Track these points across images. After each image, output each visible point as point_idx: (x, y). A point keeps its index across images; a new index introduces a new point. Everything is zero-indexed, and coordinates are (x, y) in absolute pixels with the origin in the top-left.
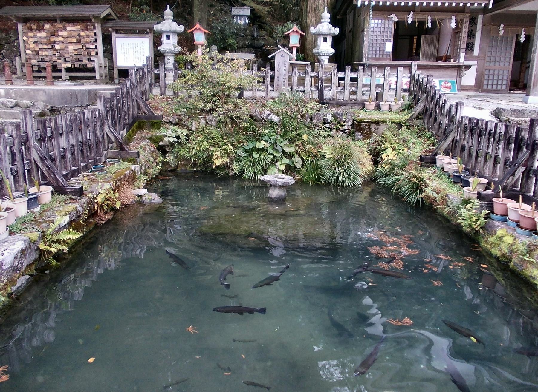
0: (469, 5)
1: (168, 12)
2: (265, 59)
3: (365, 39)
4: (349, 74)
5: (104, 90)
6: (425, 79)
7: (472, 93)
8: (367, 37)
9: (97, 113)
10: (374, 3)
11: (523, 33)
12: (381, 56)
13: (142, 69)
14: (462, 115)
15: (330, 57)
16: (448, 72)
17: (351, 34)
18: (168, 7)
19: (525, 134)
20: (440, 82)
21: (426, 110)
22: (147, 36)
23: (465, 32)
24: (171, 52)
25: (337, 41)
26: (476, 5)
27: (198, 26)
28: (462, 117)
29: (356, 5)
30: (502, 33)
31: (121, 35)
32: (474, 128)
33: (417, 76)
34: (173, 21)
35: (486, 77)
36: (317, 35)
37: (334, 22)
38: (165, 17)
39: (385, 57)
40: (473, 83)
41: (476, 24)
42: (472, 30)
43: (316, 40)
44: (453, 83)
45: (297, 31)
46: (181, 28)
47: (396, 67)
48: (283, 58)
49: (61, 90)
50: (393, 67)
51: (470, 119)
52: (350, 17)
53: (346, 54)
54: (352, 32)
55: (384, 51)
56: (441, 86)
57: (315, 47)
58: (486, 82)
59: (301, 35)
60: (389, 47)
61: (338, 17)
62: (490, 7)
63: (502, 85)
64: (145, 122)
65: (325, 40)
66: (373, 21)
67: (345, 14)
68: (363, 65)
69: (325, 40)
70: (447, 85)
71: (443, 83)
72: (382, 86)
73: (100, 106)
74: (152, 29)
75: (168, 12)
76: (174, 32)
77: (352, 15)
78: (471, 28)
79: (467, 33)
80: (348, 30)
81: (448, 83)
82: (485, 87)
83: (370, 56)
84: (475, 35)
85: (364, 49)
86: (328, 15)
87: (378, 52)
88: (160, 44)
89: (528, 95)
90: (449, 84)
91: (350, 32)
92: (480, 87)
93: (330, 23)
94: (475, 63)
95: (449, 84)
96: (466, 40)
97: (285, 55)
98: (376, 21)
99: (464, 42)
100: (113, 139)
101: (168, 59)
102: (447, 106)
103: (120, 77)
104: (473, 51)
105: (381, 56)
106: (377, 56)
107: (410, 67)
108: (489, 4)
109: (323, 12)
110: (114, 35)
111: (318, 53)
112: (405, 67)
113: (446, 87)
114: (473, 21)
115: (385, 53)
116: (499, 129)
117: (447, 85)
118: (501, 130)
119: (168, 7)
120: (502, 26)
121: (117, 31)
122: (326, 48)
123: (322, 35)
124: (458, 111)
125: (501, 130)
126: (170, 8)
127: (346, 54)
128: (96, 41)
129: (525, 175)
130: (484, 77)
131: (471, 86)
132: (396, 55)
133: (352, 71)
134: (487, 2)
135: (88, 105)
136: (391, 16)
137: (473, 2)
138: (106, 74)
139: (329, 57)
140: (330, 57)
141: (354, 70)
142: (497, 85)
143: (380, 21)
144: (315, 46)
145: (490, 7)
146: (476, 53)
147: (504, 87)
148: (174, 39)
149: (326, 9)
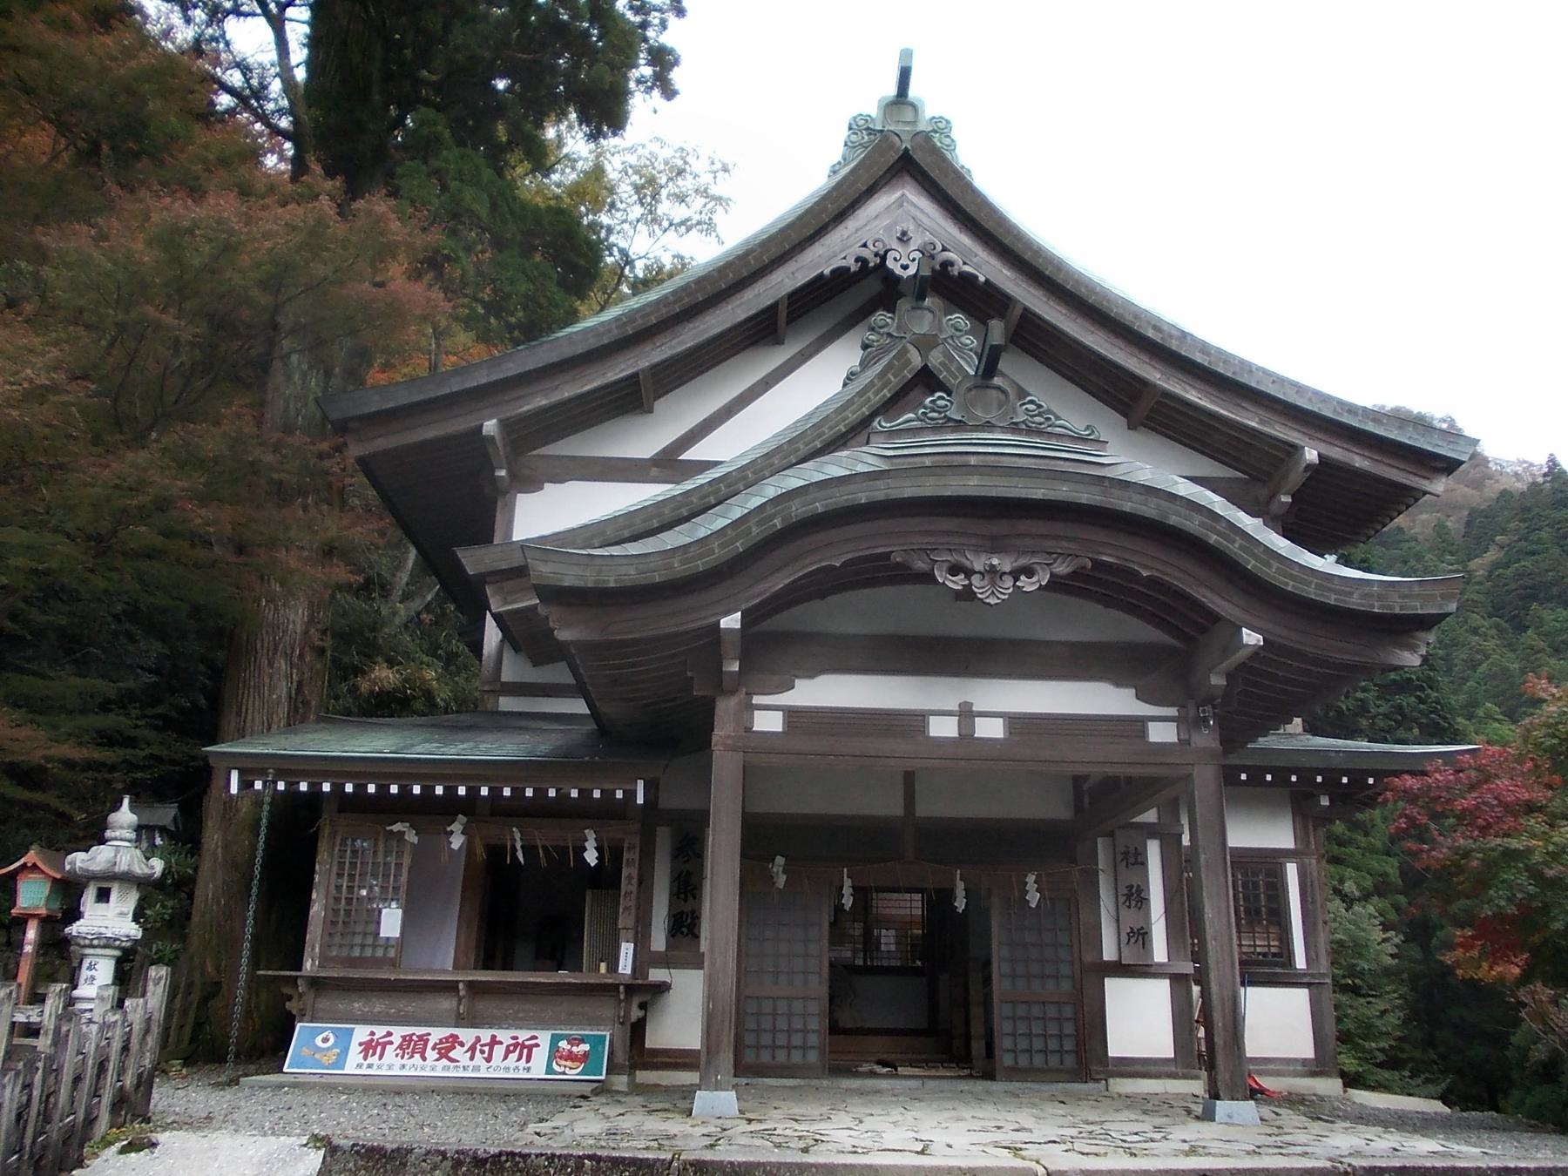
3: (314, 896)
8: (322, 890)
11: (847, 883)
16: (590, 1006)
20: (555, 1040)
24: (108, 943)
30: (781, 880)
42: (689, 874)
44: (597, 1042)
62: (640, 801)
70: (575, 1049)
71: (563, 1044)
76: (127, 878)
81: (582, 1041)
85: (311, 928)
99: (626, 908)
101: (90, 968)
104: (697, 937)
113: (571, 1057)
117: (575, 1049)
119: (126, 801)
120: (780, 860)
126: (131, 802)
136: (397, 827)
137: (587, 786)
147: (813, 1057)
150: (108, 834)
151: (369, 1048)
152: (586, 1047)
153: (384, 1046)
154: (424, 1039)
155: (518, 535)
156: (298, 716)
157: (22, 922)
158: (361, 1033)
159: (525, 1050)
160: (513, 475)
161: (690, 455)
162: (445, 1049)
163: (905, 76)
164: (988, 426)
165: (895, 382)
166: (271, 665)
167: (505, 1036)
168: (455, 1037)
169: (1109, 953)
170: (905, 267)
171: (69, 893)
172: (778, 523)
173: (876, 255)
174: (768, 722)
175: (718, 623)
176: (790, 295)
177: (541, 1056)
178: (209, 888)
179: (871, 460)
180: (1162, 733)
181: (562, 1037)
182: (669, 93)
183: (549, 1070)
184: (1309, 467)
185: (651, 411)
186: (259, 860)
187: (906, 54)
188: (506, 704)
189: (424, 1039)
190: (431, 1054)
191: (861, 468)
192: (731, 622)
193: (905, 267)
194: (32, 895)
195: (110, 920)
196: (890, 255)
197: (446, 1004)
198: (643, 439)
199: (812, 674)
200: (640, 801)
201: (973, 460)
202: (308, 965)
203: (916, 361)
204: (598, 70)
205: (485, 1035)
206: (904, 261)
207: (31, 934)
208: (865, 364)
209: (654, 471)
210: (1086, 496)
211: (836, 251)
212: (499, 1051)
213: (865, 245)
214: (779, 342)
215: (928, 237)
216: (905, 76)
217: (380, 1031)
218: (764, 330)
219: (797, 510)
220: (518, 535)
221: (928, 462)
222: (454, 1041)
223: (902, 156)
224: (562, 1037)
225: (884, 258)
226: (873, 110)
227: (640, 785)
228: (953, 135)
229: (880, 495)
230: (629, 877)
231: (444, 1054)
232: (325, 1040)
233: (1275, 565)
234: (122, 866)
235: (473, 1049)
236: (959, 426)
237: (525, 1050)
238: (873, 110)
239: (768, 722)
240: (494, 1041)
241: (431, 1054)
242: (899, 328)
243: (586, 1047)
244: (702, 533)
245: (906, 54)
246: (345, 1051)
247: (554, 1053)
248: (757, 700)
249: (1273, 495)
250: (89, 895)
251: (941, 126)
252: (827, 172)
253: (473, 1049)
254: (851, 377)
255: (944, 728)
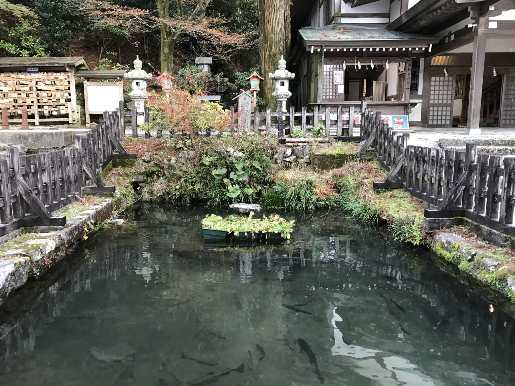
0: (410, 49)
1: (138, 63)
2: (229, 101)
4: (305, 114)
5: (81, 132)
6: (375, 116)
7: (420, 128)
9: (76, 152)
10: (325, 50)
12: (334, 97)
13: (116, 113)
14: (408, 145)
15: (288, 99)
17: (305, 80)
18: (137, 56)
19: (463, 157)
20: (393, 118)
21: (380, 144)
22: (118, 83)
23: (409, 74)
25: (293, 85)
26: (417, 49)
27: (165, 74)
28: (408, 147)
29: (310, 52)
31: (92, 83)
32: (419, 155)
33: (366, 113)
34: (142, 69)
35: (431, 113)
36: (276, 79)
37: (289, 68)
38: (134, 67)
39: (337, 97)
40: (419, 120)
41: (419, 67)
42: (415, 72)
43: (273, 85)
45: (257, 77)
46: (150, 76)
47: (348, 106)
48: (246, 101)
49: (13, 133)
50: (345, 106)
51: (415, 147)
52: (305, 64)
53: (302, 96)
54: (306, 77)
55: (336, 92)
56: (394, 122)
57: (274, 90)
58: (431, 118)
59: (261, 80)
60: (341, 89)
61: (293, 64)
62: (430, 51)
63: (446, 120)
64: (121, 159)
65: (283, 84)
66: (325, 66)
67: (300, 61)
68: (319, 105)
69: (283, 84)
70: (399, 121)
71: (396, 119)
72: (348, 122)
73: (78, 145)
74: (121, 77)
75: (138, 63)
77: (306, 62)
78: (414, 70)
79: (410, 75)
80: (303, 76)
81: (400, 118)
82: (430, 122)
83: (324, 97)
84: (418, 76)
86: (285, 62)
87: (331, 94)
88: (130, 90)
89: (469, 128)
90: (401, 121)
91: (305, 77)
92: (426, 123)
93: (286, 69)
94: (420, 101)
95: (401, 121)
96: (410, 81)
97: (247, 97)
98: (328, 66)
100: (90, 176)
102: (395, 138)
103: (91, 122)
104: (417, 90)
105: (334, 97)
106: (331, 97)
107: (361, 106)
108: (429, 48)
109: (280, 59)
110: (86, 83)
111: (277, 95)
112: (356, 106)
113: (398, 123)
114: (415, 65)
115: (337, 94)
116: (440, 154)
117: (399, 121)
118: (442, 155)
119: (137, 56)
121: (88, 79)
122: (283, 91)
123: (280, 79)
124: (405, 141)
125: (442, 155)
127: (302, 96)
128: (69, 88)
129: (465, 193)
130: (429, 113)
131: (418, 122)
132: (347, 95)
133: (308, 112)
134: (427, 47)
135: (64, 147)
137: (414, 47)
138: (78, 119)
139: (286, 99)
140: (288, 99)
141: (310, 109)
142: (441, 120)
143: (332, 66)
144: (273, 89)
145: (430, 51)
146: (420, 92)
147: (448, 122)
148: (144, 85)
149: (282, 56)
150: (279, 67)
188: (344, 21)
224: (395, 117)
227: (431, 46)
234: (142, 77)
239: (493, 25)
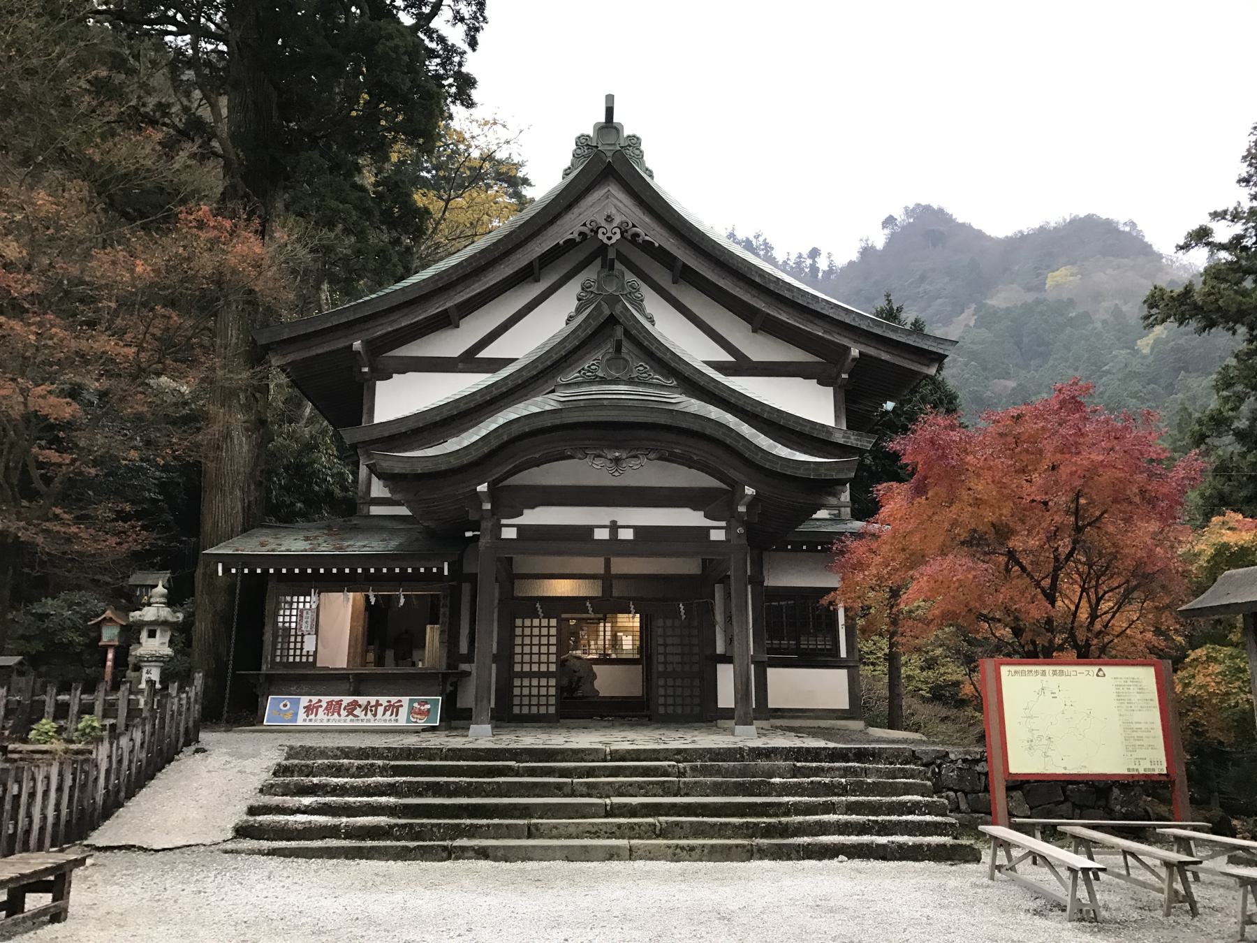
20: (411, 702)
62: (446, 573)
71: (416, 705)
76: (165, 624)
81: (426, 702)
113: (421, 713)
151: (308, 709)
152: (428, 706)
153: (317, 708)
154: (339, 703)
155: (378, 419)
156: (249, 525)
157: (105, 649)
158: (304, 700)
159: (395, 709)
160: (372, 370)
161: (485, 354)
162: (351, 708)
163: (610, 112)
164: (616, 381)
165: (594, 324)
166: (231, 493)
167: (383, 700)
168: (356, 702)
169: (720, 649)
170: (610, 238)
171: (131, 633)
172: (505, 438)
173: (592, 230)
174: (509, 533)
175: (54, 900)
176: (540, 250)
177: (404, 712)
178: (202, 627)
179: (552, 403)
180: (718, 535)
181: (415, 701)
182: (469, 104)
183: (408, 721)
184: (854, 359)
185: (458, 327)
186: (236, 612)
187: (610, 98)
189: (339, 703)
190: (344, 713)
191: (548, 408)
192: (483, 488)
193: (610, 238)
194: (109, 635)
195: (155, 646)
196: (601, 230)
197: (345, 686)
198: (451, 344)
199: (533, 507)
200: (446, 573)
201: (605, 402)
202: (264, 667)
203: (607, 312)
204: (418, 89)
205: (373, 700)
206: (609, 234)
207: (110, 656)
208: (579, 310)
209: (460, 366)
210: (662, 420)
211: (569, 228)
212: (381, 710)
213: (585, 225)
214: (537, 280)
215: (624, 219)
216: (610, 112)
217: (315, 699)
218: (527, 275)
219: (516, 430)
220: (378, 419)
221: (582, 404)
222: (355, 705)
223: (608, 162)
224: (415, 701)
225: (596, 232)
226: (590, 131)
228: (642, 148)
229: (557, 422)
230: (444, 614)
231: (351, 713)
232: (285, 705)
233: (760, 454)
235: (366, 708)
236: (603, 381)
237: (395, 709)
238: (590, 131)
239: (509, 533)
240: (378, 704)
241: (344, 713)
242: (598, 289)
243: (428, 706)
244: (466, 443)
245: (610, 98)
246: (296, 714)
247: (412, 711)
248: (504, 521)
249: (839, 375)
250: (144, 634)
251: (634, 141)
252: (561, 174)
253: (366, 708)
254: (570, 319)
255: (602, 535)
